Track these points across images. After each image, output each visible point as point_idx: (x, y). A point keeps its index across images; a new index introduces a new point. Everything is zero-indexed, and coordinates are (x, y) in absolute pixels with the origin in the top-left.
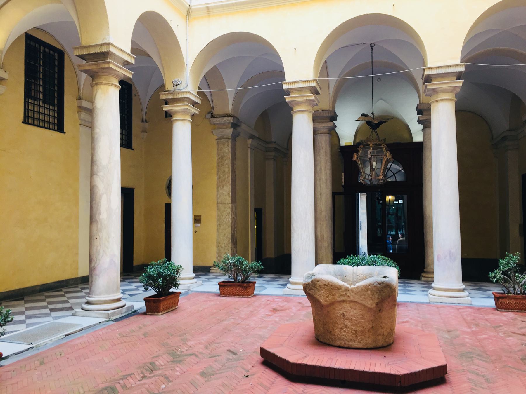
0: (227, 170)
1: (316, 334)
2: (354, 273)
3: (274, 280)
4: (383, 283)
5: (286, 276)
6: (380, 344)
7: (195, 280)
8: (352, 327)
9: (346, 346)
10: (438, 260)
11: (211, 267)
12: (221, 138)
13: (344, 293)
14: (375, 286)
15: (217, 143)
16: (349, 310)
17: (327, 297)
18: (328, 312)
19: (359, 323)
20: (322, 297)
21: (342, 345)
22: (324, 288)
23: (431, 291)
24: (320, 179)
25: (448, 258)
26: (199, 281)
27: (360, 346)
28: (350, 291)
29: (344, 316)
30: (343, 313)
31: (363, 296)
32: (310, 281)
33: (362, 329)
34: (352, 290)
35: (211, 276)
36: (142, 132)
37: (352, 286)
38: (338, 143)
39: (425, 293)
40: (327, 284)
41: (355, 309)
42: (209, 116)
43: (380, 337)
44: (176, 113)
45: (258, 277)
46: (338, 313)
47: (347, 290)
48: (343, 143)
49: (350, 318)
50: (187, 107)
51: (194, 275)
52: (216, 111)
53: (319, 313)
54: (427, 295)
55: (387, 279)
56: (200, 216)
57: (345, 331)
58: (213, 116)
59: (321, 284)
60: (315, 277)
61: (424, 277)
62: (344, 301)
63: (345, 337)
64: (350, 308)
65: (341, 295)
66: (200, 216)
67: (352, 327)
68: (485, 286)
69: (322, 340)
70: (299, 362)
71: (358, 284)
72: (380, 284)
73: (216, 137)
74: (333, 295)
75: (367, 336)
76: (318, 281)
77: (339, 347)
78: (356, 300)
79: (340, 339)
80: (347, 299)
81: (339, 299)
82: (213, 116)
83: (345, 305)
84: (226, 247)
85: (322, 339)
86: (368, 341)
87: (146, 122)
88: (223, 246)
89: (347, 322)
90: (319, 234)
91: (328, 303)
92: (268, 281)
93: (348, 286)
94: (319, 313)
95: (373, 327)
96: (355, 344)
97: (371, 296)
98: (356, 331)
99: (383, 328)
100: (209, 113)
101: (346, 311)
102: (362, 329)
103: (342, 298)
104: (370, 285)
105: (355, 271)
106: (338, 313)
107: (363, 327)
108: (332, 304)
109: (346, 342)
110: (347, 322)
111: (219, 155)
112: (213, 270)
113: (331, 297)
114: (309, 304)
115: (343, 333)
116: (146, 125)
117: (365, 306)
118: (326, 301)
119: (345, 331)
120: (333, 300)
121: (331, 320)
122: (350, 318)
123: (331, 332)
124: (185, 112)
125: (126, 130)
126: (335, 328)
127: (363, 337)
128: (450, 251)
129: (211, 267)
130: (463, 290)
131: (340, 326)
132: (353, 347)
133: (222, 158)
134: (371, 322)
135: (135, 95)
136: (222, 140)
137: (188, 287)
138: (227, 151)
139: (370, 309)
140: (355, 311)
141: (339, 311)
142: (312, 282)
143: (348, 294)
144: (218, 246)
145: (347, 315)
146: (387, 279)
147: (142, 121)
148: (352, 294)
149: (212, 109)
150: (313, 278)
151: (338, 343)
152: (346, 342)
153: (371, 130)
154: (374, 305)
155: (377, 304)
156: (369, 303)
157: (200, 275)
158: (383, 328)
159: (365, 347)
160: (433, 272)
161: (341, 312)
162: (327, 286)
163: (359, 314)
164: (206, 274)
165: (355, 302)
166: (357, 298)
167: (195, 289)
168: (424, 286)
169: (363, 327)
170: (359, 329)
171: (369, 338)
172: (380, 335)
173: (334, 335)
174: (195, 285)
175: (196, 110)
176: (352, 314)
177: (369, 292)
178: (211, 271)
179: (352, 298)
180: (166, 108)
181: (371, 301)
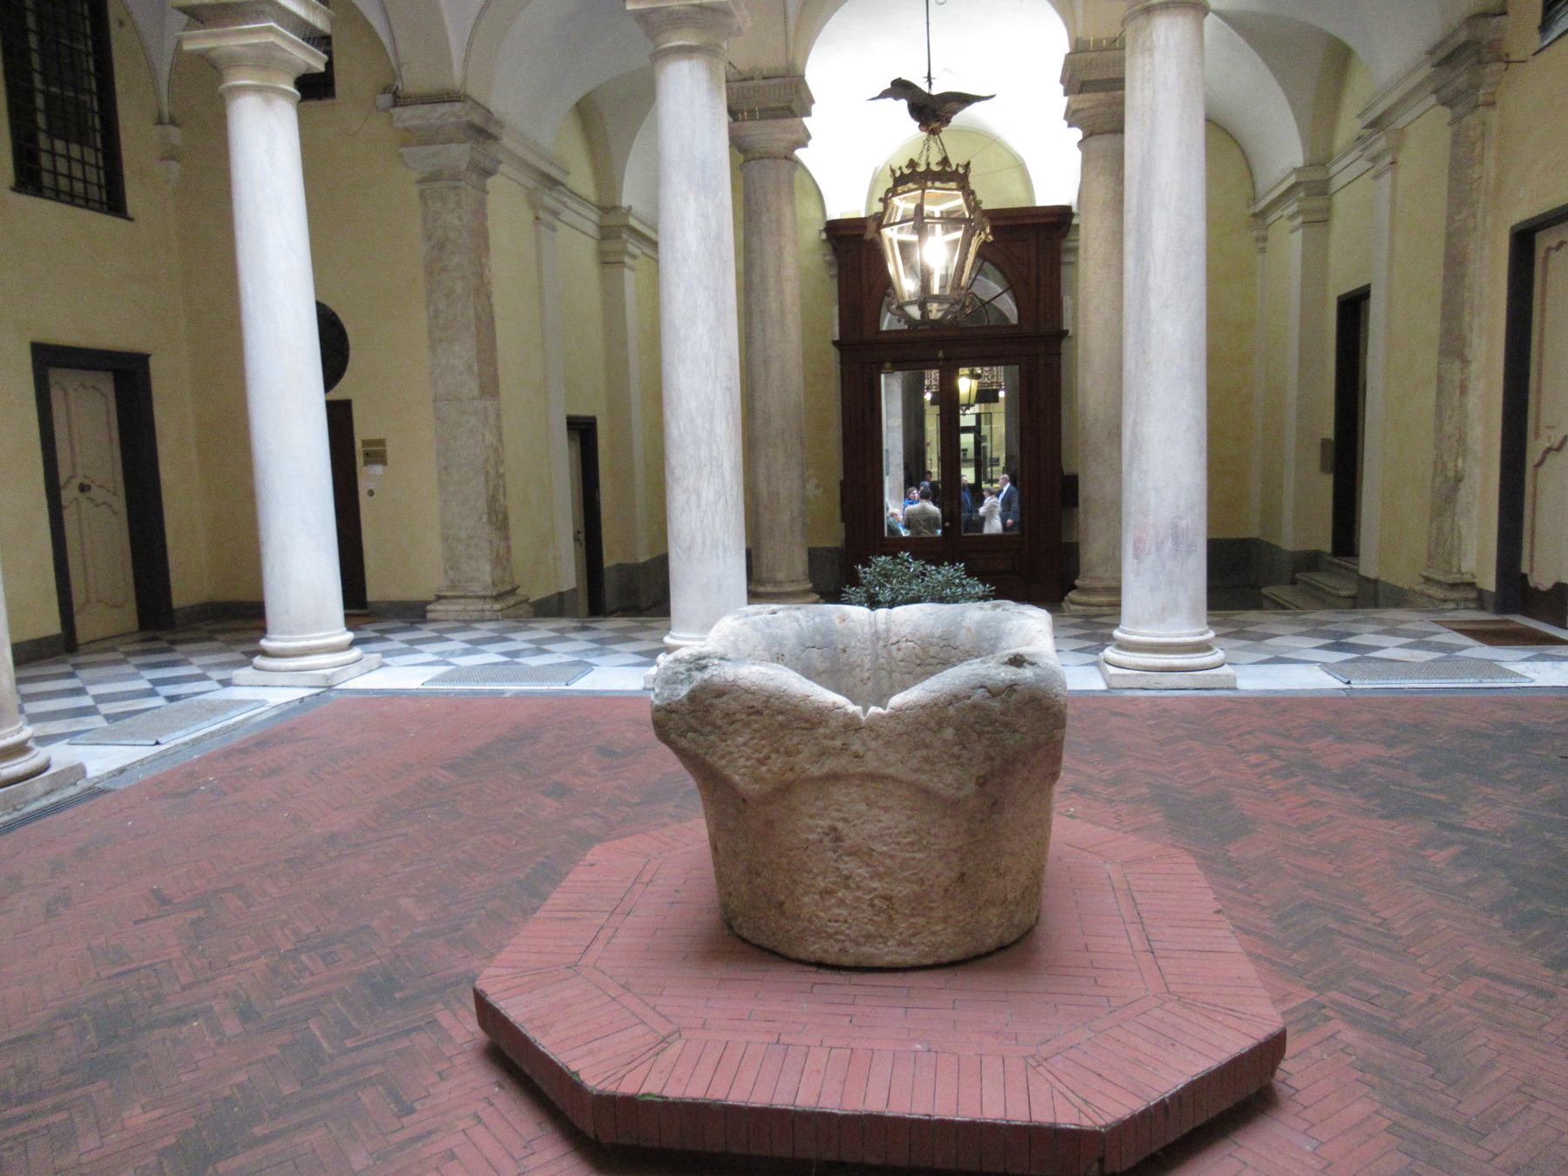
0: (459, 287)
1: (724, 905)
2: (876, 635)
3: (624, 637)
4: (1011, 687)
5: (657, 623)
6: (991, 942)
7: (356, 652)
8: (875, 884)
9: (847, 960)
10: (1136, 556)
11: (429, 603)
12: (434, 177)
13: (838, 743)
14: (974, 706)
15: (422, 196)
16: (860, 816)
17: (762, 762)
18: (769, 823)
19: (901, 868)
20: (741, 762)
21: (831, 958)
22: (747, 724)
23: (1110, 653)
24: (762, 312)
25: (1169, 545)
26: (76, 761)
27: (910, 957)
28: (865, 733)
29: (838, 839)
30: (835, 829)
31: (924, 753)
32: (683, 691)
33: (916, 888)
34: (872, 727)
35: (426, 631)
36: (162, 159)
37: (873, 710)
38: (818, 215)
39: (1091, 658)
40: (758, 705)
41: (886, 809)
42: (387, 99)
43: (993, 912)
44: (235, 61)
45: (576, 630)
46: (811, 829)
47: (851, 725)
48: (835, 212)
49: (870, 844)
50: (272, 38)
51: (350, 636)
52: (414, 80)
53: (731, 824)
54: (1096, 664)
55: (1027, 673)
56: (382, 442)
57: (841, 902)
58: (398, 100)
59: (734, 706)
60: (706, 675)
61: (1072, 602)
62: (834, 777)
63: (843, 927)
64: (863, 807)
65: (824, 753)
66: (382, 442)
67: (875, 884)
68: (1252, 624)
69: (745, 933)
70: (628, 1087)
71: (897, 700)
72: (994, 693)
73: (416, 176)
74: (788, 754)
75: (940, 914)
76: (720, 693)
77: (820, 965)
78: (891, 771)
79: (819, 933)
80: (852, 769)
81: (815, 771)
82: (398, 100)
83: (839, 793)
84: (470, 538)
85: (750, 933)
86: (943, 937)
87: (173, 122)
88: (463, 535)
89: (851, 866)
90: (762, 486)
91: (768, 788)
92: (602, 641)
93: (852, 708)
94: (731, 824)
95: (962, 877)
96: (889, 953)
97: (956, 750)
98: (888, 898)
99: (1001, 875)
100: (385, 90)
101: (845, 820)
102: (916, 888)
103: (830, 765)
104: (954, 698)
105: (881, 627)
106: (811, 829)
107: (922, 881)
108: (785, 790)
109: (848, 944)
110: (851, 866)
111: (429, 238)
112: (436, 609)
113: (777, 762)
114: (692, 783)
115: (833, 913)
116: (175, 134)
117: (926, 792)
118: (759, 779)
119: (841, 902)
120: (790, 776)
121: (781, 855)
122: (870, 844)
123: (782, 904)
124: (265, 60)
125: (96, 150)
126: (800, 890)
127: (922, 921)
128: (1175, 526)
129: (429, 603)
130: (1203, 647)
131: (821, 883)
132: (879, 963)
133: (441, 246)
134: (955, 859)
135: (121, 23)
136: (437, 185)
137: (327, 678)
138: (456, 222)
139: (952, 806)
140: (885, 817)
141: (811, 821)
142: (693, 697)
143: (857, 746)
144: (445, 539)
145: (852, 837)
146: (1027, 673)
147: (160, 122)
148: (873, 744)
149: (395, 75)
150: (698, 677)
151: (814, 949)
152: (848, 944)
153: (925, 134)
154: (971, 788)
155: (982, 782)
156: (949, 778)
157: (391, 631)
158: (1001, 875)
159: (929, 961)
160: (1117, 591)
161: (825, 823)
162: (759, 713)
163: (903, 827)
164: (411, 627)
165: (884, 778)
166: (896, 764)
167: (351, 685)
168: (1082, 632)
169: (922, 881)
170: (902, 890)
171: (945, 920)
172: (990, 902)
173: (797, 918)
174: (354, 669)
175: (310, 52)
176: (871, 828)
177: (949, 733)
178: (429, 616)
179: (872, 764)
180: (200, 41)
181: (957, 771)
